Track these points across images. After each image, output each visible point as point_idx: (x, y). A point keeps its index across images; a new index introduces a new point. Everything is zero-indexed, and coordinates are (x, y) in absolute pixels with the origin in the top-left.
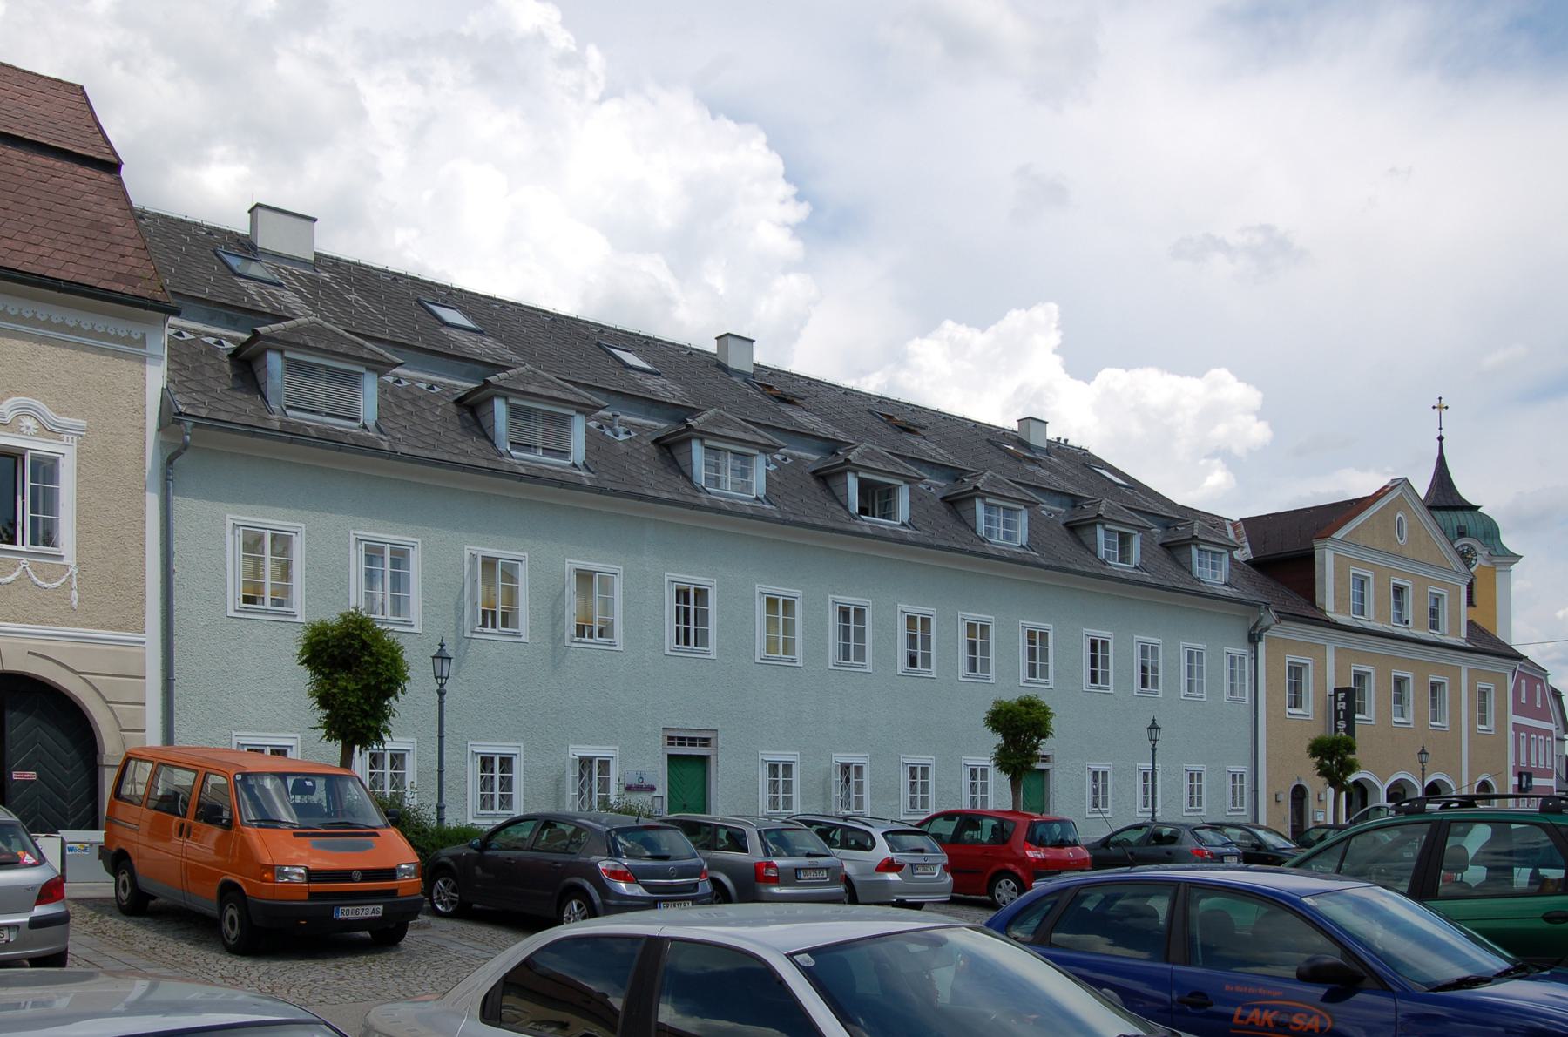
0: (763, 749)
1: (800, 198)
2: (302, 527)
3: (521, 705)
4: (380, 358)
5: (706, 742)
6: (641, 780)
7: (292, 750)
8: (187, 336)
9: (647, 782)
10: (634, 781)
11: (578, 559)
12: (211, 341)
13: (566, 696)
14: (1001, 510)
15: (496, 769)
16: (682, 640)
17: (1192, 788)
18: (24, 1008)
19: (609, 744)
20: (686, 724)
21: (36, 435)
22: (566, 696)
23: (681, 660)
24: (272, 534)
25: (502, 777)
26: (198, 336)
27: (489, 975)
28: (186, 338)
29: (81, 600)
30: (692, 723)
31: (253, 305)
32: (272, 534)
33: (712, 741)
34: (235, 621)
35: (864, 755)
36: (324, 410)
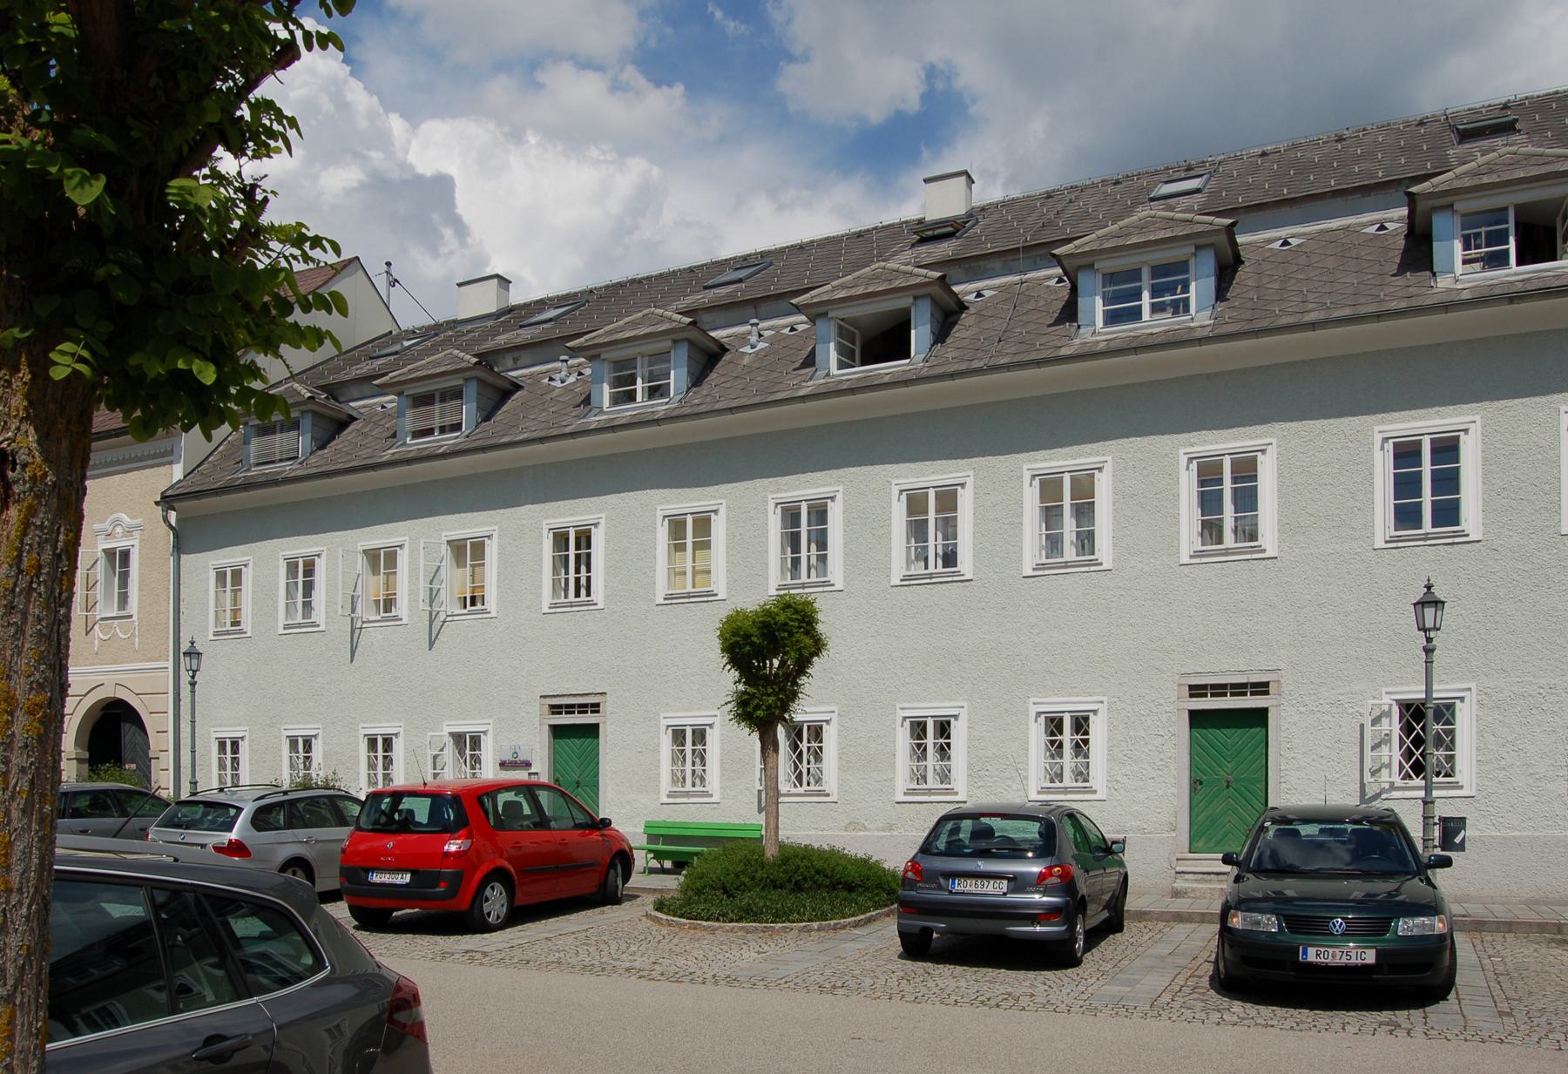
0: (285, 723)
1: (95, 172)
2: (494, 530)
3: (402, 685)
4: (1210, 228)
5: (1261, 688)
6: (515, 756)
7: (242, 740)
8: (1294, 242)
9: (522, 757)
10: (508, 757)
11: (455, 530)
12: (1372, 229)
13: (441, 672)
14: (1038, 258)
15: (467, 744)
16: (583, 592)
17: (235, 767)
18: (218, 916)
19: (484, 718)
20: (567, 689)
21: (122, 537)
22: (441, 672)
23: (561, 616)
24: (1431, 439)
25: (683, 745)
26: (777, 330)
27: (1441, 1016)
28: (800, 330)
29: (139, 643)
30: (572, 686)
31: (1533, 141)
32: (1431, 439)
33: (1272, 688)
34: (1385, 552)
35: (398, 725)
36: (278, 457)
